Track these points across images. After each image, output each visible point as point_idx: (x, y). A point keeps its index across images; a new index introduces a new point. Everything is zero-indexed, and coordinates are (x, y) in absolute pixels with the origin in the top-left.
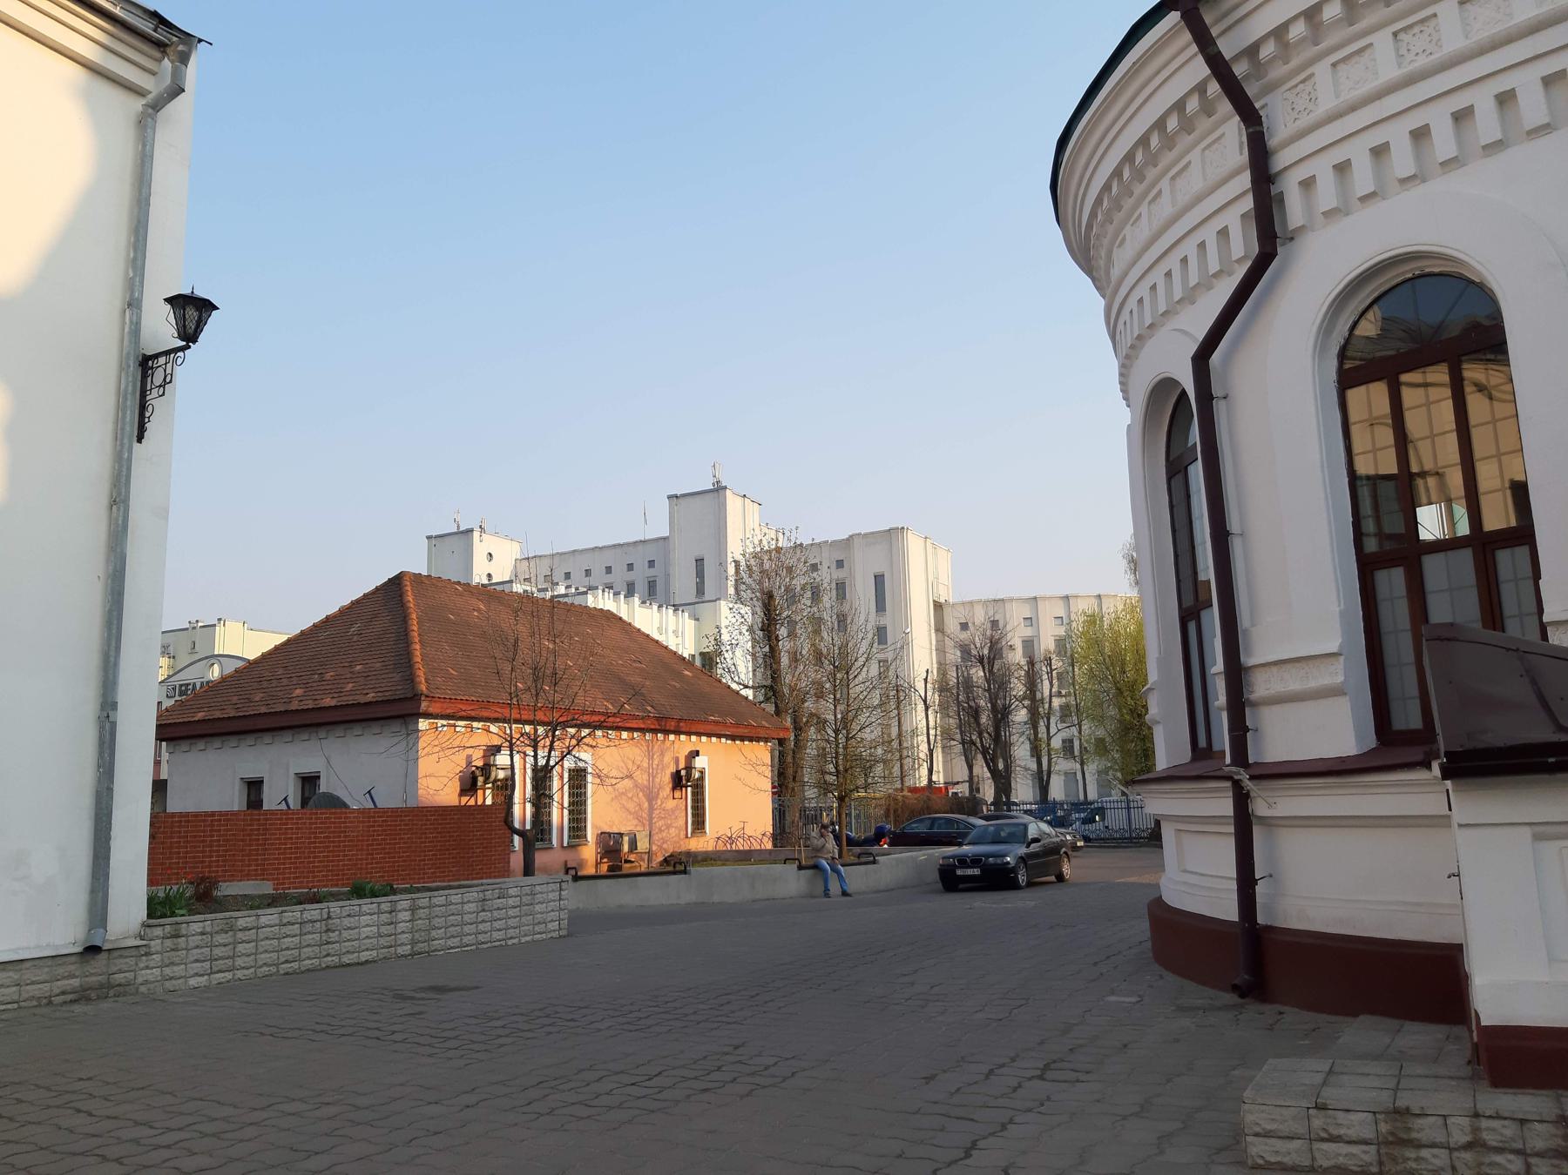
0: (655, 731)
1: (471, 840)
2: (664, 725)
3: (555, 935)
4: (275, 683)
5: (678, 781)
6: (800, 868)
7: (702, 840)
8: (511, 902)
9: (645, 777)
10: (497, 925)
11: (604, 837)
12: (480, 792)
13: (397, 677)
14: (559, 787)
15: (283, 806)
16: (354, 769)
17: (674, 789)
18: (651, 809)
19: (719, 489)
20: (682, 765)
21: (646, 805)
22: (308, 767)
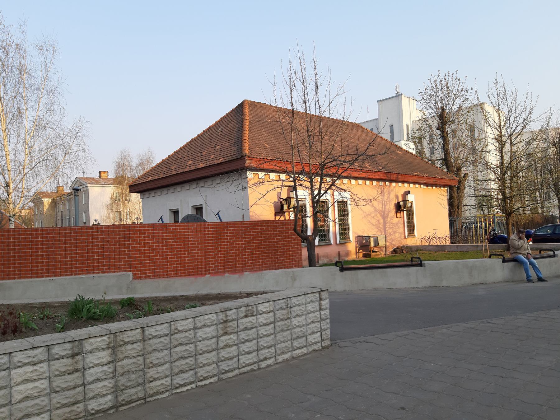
0: (384, 180)
1: (285, 241)
2: (389, 177)
3: (317, 347)
4: (182, 160)
5: (399, 208)
6: (504, 261)
7: (413, 239)
8: (262, 319)
9: (381, 205)
10: (245, 347)
11: (360, 238)
12: (287, 214)
13: (235, 148)
14: (333, 213)
15: (161, 222)
16: (218, 202)
17: (397, 212)
18: (385, 223)
19: (399, 95)
20: (400, 199)
21: (382, 221)
22: (197, 203)
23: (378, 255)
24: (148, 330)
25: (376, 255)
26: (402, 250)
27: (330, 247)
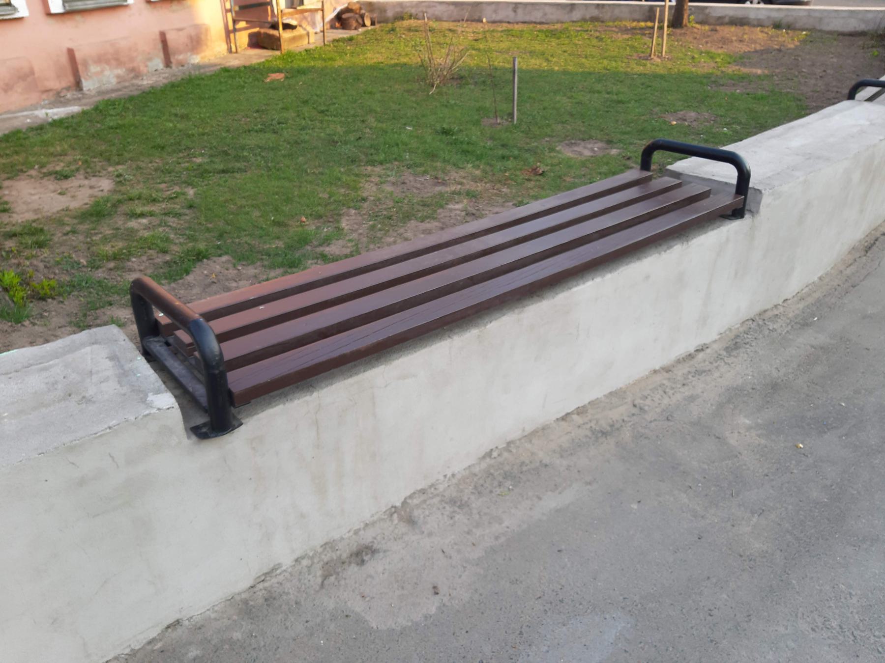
23: (300, 37)
24: (105, 314)
25: (294, 39)
26: (362, 17)
27: (121, 16)
